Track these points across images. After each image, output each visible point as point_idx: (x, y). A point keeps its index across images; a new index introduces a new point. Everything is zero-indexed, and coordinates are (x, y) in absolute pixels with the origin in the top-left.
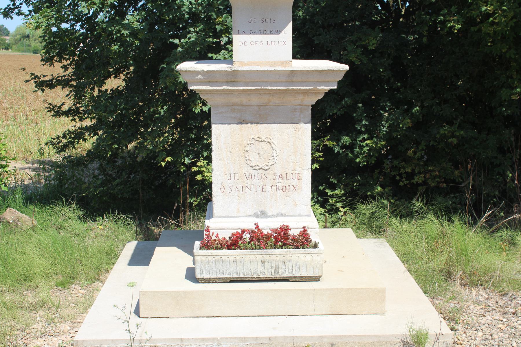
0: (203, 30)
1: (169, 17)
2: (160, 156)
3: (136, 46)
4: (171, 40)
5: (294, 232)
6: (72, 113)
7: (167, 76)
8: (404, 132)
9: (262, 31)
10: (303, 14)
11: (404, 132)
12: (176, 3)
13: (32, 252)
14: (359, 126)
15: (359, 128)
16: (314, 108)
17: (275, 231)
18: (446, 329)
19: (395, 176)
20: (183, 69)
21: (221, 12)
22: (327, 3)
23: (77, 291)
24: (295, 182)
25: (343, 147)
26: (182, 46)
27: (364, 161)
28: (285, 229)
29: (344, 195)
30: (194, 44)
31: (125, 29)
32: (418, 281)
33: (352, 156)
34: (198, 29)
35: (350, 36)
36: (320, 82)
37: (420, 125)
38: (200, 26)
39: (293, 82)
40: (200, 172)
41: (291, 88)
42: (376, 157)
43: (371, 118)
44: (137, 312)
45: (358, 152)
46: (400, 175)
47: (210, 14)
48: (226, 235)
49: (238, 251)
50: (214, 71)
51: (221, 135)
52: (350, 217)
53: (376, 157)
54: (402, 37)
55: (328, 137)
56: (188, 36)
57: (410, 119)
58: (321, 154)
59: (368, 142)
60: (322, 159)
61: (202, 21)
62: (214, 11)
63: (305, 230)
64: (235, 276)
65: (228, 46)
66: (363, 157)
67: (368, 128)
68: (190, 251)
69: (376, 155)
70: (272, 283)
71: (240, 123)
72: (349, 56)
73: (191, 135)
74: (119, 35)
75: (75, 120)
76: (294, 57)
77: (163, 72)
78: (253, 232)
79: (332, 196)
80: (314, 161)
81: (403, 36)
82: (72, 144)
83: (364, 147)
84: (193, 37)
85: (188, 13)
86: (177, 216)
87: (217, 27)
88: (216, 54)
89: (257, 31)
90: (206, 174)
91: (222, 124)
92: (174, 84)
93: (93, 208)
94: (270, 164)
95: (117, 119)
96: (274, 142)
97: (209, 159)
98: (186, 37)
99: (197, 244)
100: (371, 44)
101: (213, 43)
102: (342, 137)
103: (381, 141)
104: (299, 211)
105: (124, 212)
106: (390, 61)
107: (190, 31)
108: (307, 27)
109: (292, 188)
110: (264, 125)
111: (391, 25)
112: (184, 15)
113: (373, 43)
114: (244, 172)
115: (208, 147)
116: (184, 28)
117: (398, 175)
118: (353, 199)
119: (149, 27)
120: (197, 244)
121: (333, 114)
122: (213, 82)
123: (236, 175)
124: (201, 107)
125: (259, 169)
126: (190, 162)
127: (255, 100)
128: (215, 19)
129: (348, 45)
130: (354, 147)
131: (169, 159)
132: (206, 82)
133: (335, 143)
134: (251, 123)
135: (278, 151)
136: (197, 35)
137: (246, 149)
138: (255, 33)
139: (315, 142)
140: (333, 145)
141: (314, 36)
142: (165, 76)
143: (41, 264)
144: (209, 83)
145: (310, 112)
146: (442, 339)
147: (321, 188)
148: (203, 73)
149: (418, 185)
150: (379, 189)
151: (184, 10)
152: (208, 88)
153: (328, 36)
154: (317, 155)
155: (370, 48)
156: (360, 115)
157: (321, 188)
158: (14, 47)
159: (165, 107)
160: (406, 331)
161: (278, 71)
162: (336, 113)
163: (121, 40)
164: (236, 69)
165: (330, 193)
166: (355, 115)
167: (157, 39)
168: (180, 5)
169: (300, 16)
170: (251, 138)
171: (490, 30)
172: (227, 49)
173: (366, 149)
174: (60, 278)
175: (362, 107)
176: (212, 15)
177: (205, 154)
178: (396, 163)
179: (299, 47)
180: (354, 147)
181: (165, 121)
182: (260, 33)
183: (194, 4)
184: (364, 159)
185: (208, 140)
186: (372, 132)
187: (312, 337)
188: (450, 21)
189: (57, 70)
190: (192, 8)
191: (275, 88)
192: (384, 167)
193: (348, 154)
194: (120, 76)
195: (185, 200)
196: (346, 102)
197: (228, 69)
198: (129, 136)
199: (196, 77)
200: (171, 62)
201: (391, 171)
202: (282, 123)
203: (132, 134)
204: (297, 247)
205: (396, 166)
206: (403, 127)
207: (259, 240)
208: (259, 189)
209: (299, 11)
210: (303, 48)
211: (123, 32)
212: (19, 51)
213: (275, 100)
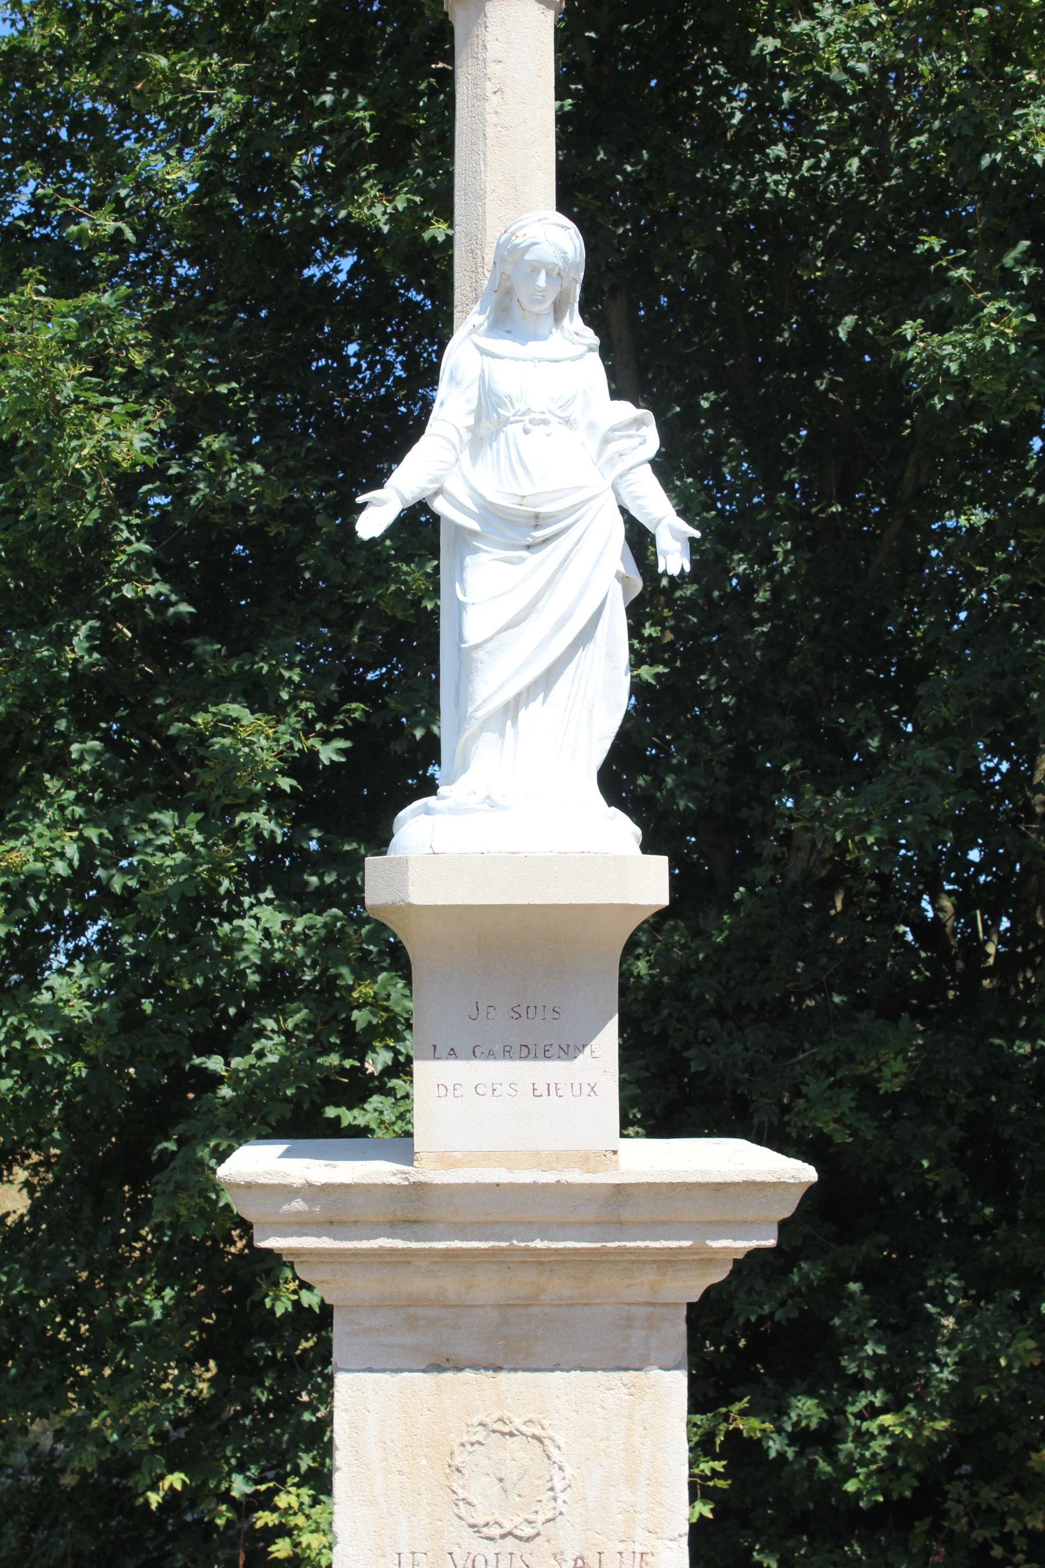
0: (309, 1026)
1: (190, 982)
2: (145, 1469)
3: (75, 1080)
4: (197, 1061)
7: (180, 1187)
8: (1014, 1385)
9: (516, 1048)
10: (651, 967)
11: (1014, 1385)
12: (216, 936)
14: (852, 1359)
15: (852, 1368)
16: (696, 1313)
19: (986, 1546)
20: (240, 1180)
21: (372, 963)
22: (731, 933)
25: (800, 1437)
27: (873, 1491)
30: (278, 1072)
31: (41, 1024)
33: (829, 1469)
34: (290, 1025)
35: (813, 1045)
36: (718, 1223)
38: (298, 1011)
39: (621, 1223)
40: (283, 1531)
41: (616, 1244)
42: (918, 1476)
43: (895, 1329)
45: (850, 1456)
46: (1006, 1539)
47: (332, 971)
50: (347, 1186)
51: (367, 1408)
53: (918, 1476)
54: (992, 1045)
55: (744, 1404)
56: (256, 1047)
57: (1031, 1337)
58: (719, 1466)
59: (887, 1419)
60: (722, 1484)
61: (306, 994)
62: (347, 962)
65: (394, 1083)
66: (869, 1476)
67: (885, 1367)
69: (918, 1467)
71: (436, 1368)
72: (811, 1114)
73: (258, 1392)
74: (17, 1044)
77: (167, 1173)
80: (698, 1489)
81: (997, 1041)
83: (873, 1437)
84: (272, 1050)
85: (258, 969)
87: (356, 1014)
88: (350, 1108)
89: (497, 1048)
90: (305, 1539)
91: (370, 1370)
92: (202, 1212)
94: (541, 1518)
96: (557, 1437)
97: (320, 1482)
98: (248, 1050)
100: (887, 1072)
101: (342, 1071)
102: (793, 1401)
103: (933, 1419)
106: (955, 1133)
107: (264, 1028)
108: (666, 1012)
110: (521, 1375)
111: (624, 173)
112: (243, 974)
114: (447, 1548)
115: (319, 1437)
116: (243, 1016)
117: (996, 1540)
119: (121, 1014)
121: (761, 1320)
122: (342, 1223)
123: (420, 1557)
124: (295, 1292)
125: (503, 1536)
126: (249, 1489)
127: (488, 1287)
128: (352, 988)
129: (808, 1078)
130: (838, 1436)
131: (176, 1480)
132: (318, 1224)
133: (768, 1426)
134: (475, 1367)
135: (569, 1471)
136: (286, 1045)
137: (457, 1461)
138: (490, 1055)
139: (697, 1418)
140: (764, 1431)
141: (687, 1046)
142: (172, 1185)
144: (329, 1226)
145: (683, 1327)
148: (311, 1192)
151: (246, 958)
152: (325, 1243)
153: (738, 1047)
154: (705, 1467)
155: (884, 1087)
156: (858, 1322)
159: (168, 1293)
161: (569, 1185)
162: (772, 1314)
164: (423, 1179)
166: (837, 1321)
167: (149, 1055)
168: (233, 940)
169: (639, 977)
170: (475, 1421)
172: (390, 1092)
173: (879, 1446)
175: (863, 1292)
176: (339, 976)
177: (306, 1462)
178: (988, 1494)
179: (638, 1082)
180: (838, 1436)
181: (166, 1344)
182: (507, 1053)
183: (280, 938)
184: (873, 1481)
185: (315, 1410)
186: (900, 1387)
190: (273, 950)
191: (560, 1245)
192: (948, 1511)
193: (815, 1463)
194: (10, 1173)
196: (804, 1277)
197: (394, 1180)
198: (36, 1397)
199: (285, 1208)
200: (194, 1137)
201: (971, 1525)
202: (583, 1369)
203: (47, 1388)
205: (990, 1509)
206: (1009, 1366)
209: (638, 957)
210: (656, 1103)
211: (33, 1033)
213: (560, 1286)
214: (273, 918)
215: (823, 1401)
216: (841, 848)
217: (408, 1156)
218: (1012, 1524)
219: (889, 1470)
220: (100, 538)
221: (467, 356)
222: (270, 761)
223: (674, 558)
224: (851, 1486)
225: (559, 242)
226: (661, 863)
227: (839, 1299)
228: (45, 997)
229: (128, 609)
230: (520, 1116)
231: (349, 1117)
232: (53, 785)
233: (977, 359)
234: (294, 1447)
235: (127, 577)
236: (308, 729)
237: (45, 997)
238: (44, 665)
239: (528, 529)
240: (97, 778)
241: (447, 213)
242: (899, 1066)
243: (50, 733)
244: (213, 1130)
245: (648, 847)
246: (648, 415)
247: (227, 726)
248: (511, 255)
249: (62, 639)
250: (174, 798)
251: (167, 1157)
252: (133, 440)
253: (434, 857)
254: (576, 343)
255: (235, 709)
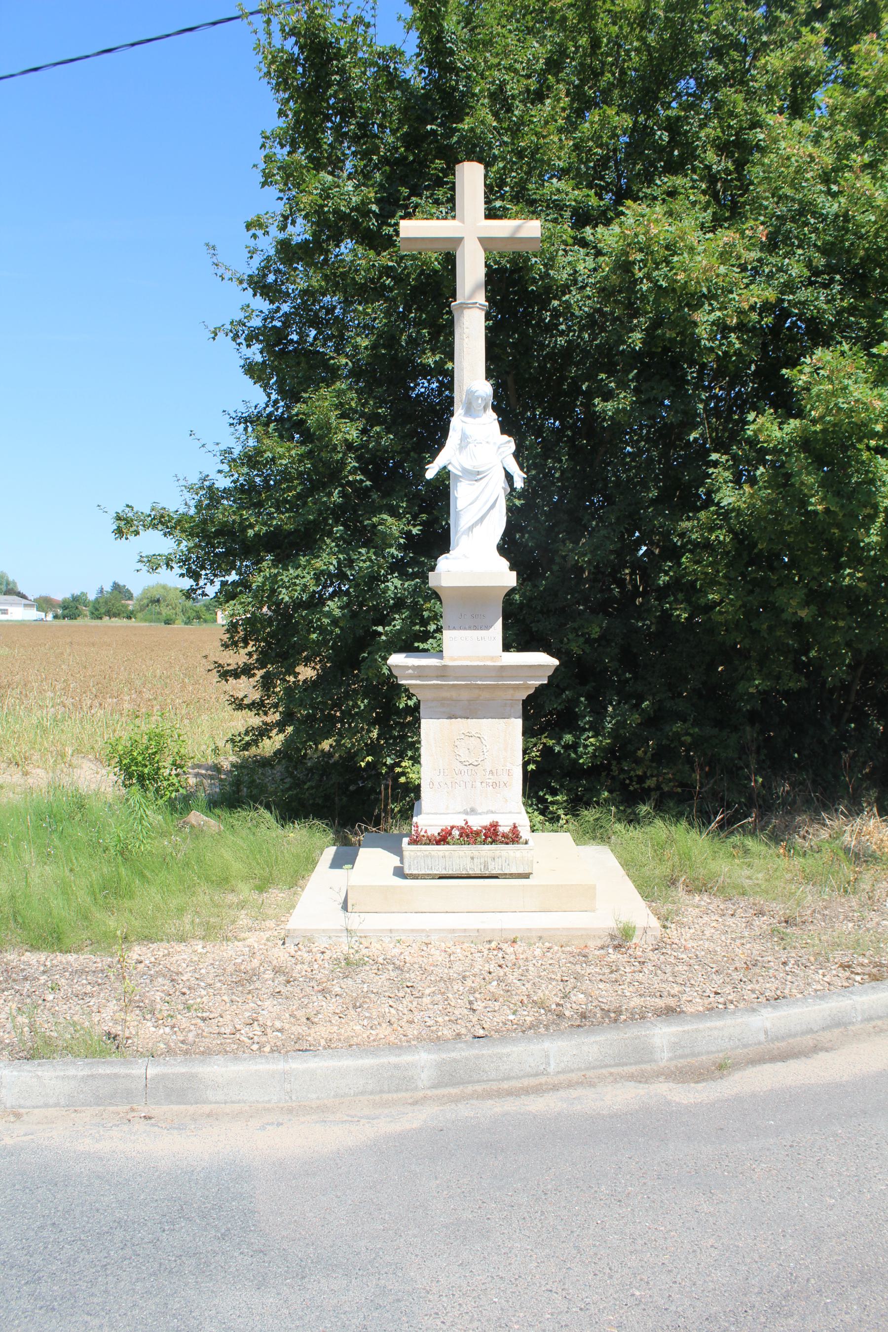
0: (409, 617)
5: (504, 829)
6: (258, 706)
7: (370, 667)
13: (227, 855)
17: (485, 828)
18: (655, 923)
23: (276, 895)
24: (505, 778)
25: (567, 747)
26: (386, 634)
28: (495, 825)
29: (566, 801)
30: (399, 632)
32: (639, 887)
37: (653, 721)
40: (403, 774)
44: (345, 907)
46: (630, 778)
48: (434, 831)
49: (446, 847)
51: (432, 731)
52: (573, 824)
59: (592, 740)
61: (408, 607)
63: (515, 827)
64: (444, 872)
68: (399, 852)
70: (482, 880)
75: (258, 714)
76: (507, 647)
78: (463, 828)
79: (553, 803)
82: (255, 742)
84: (398, 624)
86: (377, 824)
93: (291, 811)
95: (307, 714)
97: (416, 760)
99: (406, 840)
104: (510, 807)
105: (319, 816)
109: (502, 784)
113: (595, 632)
115: (415, 746)
118: (575, 805)
120: (406, 840)
138: (465, 629)
143: (237, 867)
144: (418, 677)
146: (649, 933)
147: (541, 794)
148: (414, 668)
149: (650, 789)
150: (606, 794)
152: (418, 682)
157: (541, 794)
158: (139, 615)
160: (612, 924)
163: (322, 629)
165: (550, 798)
171: (721, 619)
173: (591, 749)
174: (257, 882)
177: (410, 753)
182: (470, 628)
187: (520, 930)
188: (677, 609)
189: (238, 658)
195: (386, 805)
204: (507, 843)
207: (469, 836)
208: (469, 785)
212: (146, 621)
213: (485, 695)
214: (398, 583)
215: (574, 736)
216: (577, 561)
217: (442, 658)
218: (632, 773)
219: (594, 756)
220: (342, 463)
221: (458, 423)
222: (397, 534)
223: (519, 484)
224: (581, 761)
225: (485, 389)
226: (515, 573)
227: (577, 703)
228: (327, 609)
229: (350, 483)
230: (474, 646)
231: (422, 646)
232: (328, 541)
233: (618, 411)
234: (406, 750)
235: (350, 473)
236: (409, 523)
237: (327, 609)
238: (325, 502)
239: (476, 475)
240: (342, 537)
241: (452, 359)
242: (598, 629)
243: (327, 524)
244: (379, 650)
245: (511, 569)
246: (511, 439)
247: (382, 522)
248: (470, 393)
249: (330, 494)
250: (367, 544)
251: (364, 659)
252: (351, 432)
253: (450, 571)
254: (491, 418)
255: (385, 516)
